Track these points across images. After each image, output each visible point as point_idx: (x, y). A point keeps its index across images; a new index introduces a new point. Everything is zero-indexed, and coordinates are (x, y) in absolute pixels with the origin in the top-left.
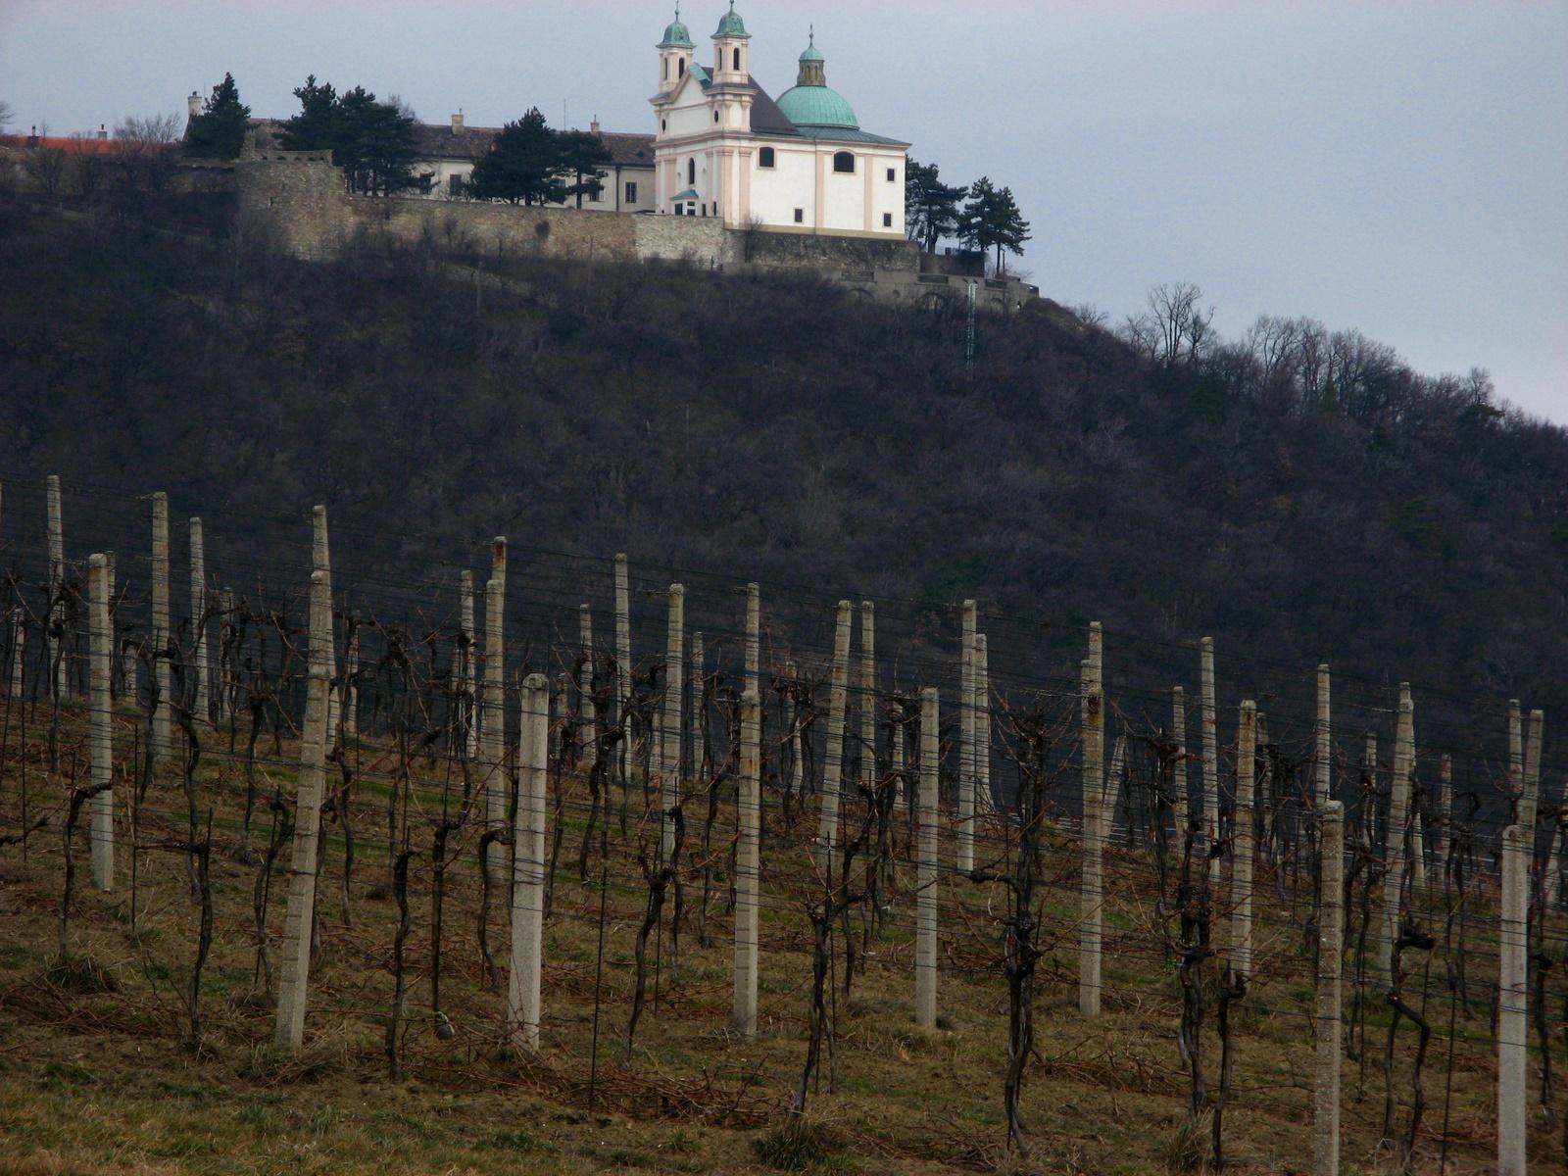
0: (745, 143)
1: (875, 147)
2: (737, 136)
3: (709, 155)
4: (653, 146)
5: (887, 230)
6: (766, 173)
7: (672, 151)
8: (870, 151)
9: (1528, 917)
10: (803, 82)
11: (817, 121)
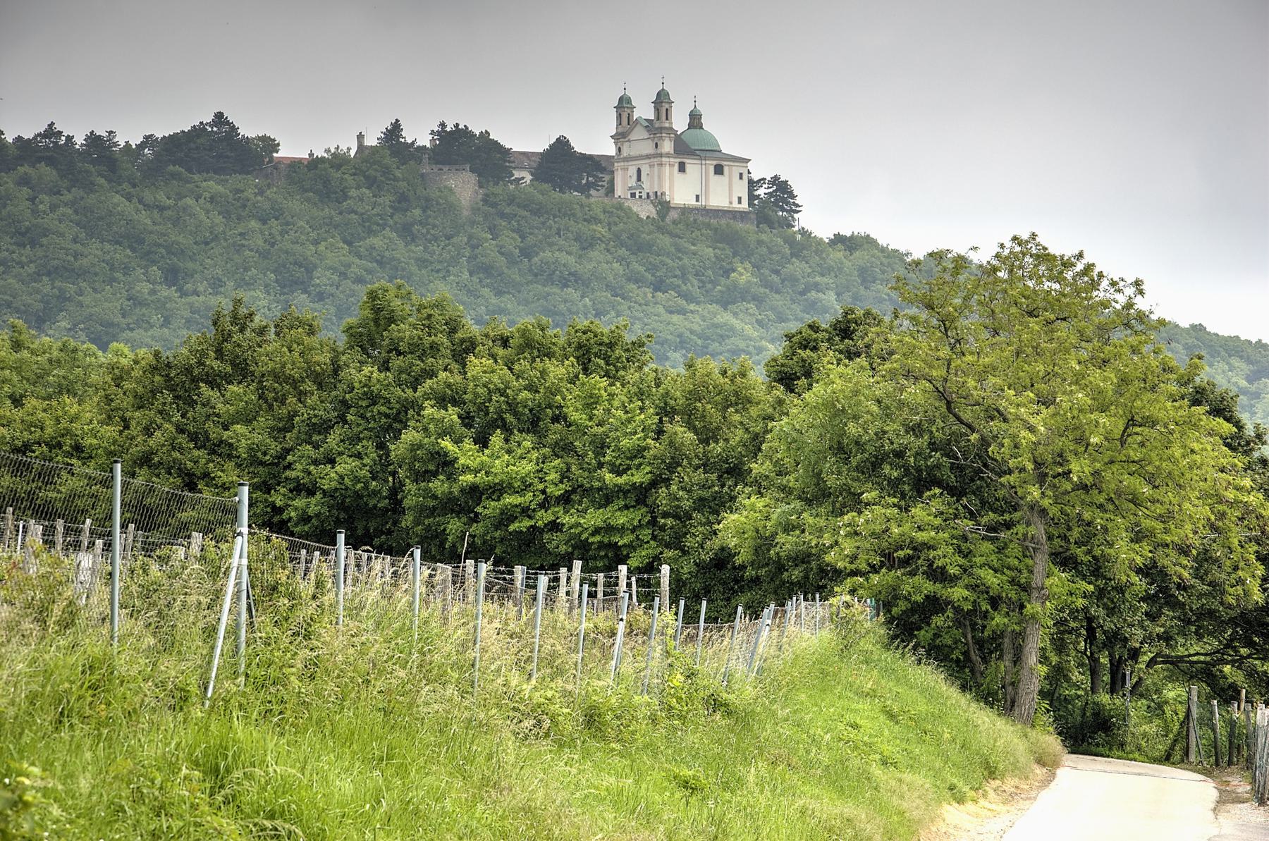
0: (672, 160)
1: (734, 161)
2: (668, 155)
3: (651, 166)
4: (613, 160)
5: (739, 206)
6: (681, 175)
7: (626, 163)
8: (732, 164)
9: (1089, 755)
10: (691, 126)
11: (703, 148)
